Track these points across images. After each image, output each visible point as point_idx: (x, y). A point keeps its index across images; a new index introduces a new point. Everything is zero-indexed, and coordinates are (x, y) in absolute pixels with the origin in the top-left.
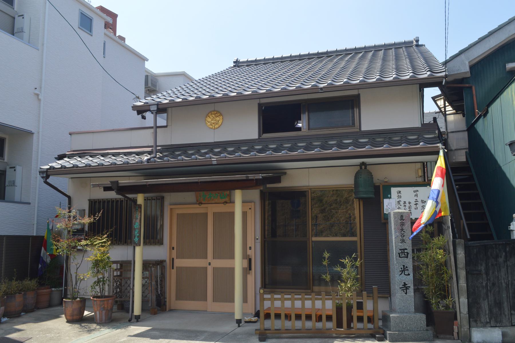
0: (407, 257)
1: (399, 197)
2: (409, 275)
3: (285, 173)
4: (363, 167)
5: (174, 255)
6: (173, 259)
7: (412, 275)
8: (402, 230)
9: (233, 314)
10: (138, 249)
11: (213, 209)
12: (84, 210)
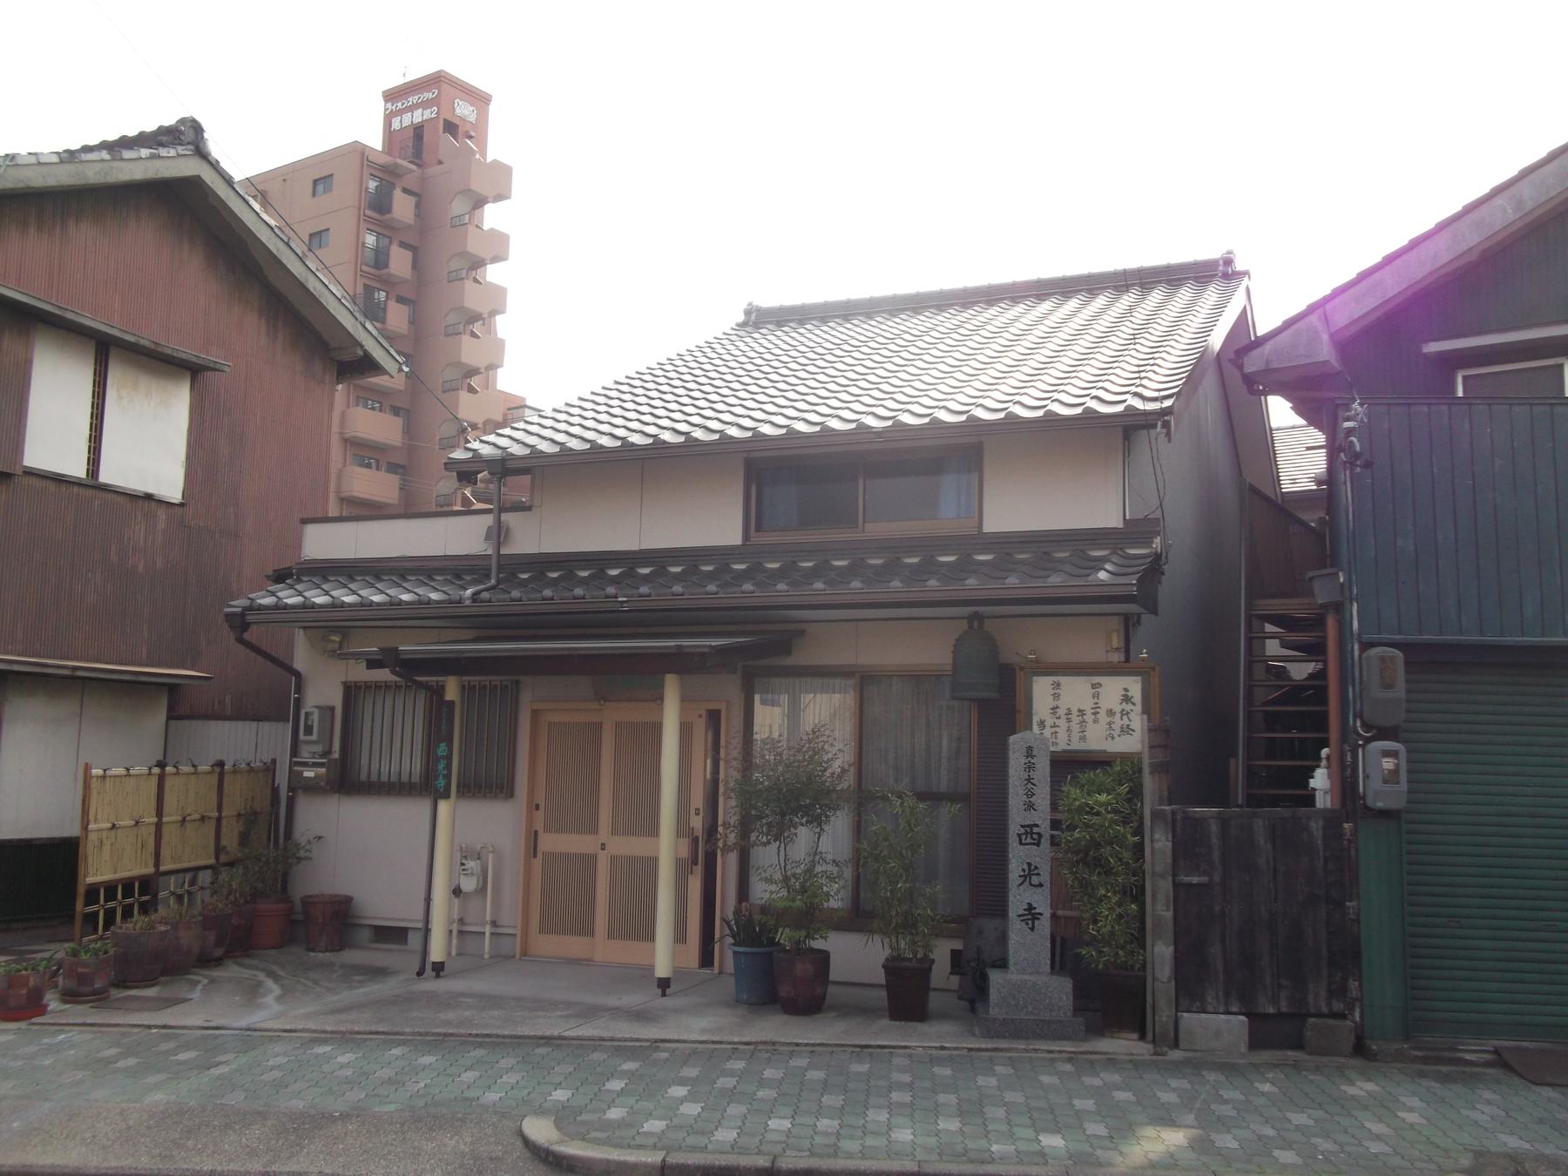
0: (1038, 845)
1: (1056, 696)
2: (1041, 885)
3: (802, 633)
4: (976, 624)
5: (539, 826)
6: (536, 833)
7: (1047, 884)
8: (1029, 780)
9: (652, 968)
10: (443, 806)
11: (613, 715)
12: (332, 709)
